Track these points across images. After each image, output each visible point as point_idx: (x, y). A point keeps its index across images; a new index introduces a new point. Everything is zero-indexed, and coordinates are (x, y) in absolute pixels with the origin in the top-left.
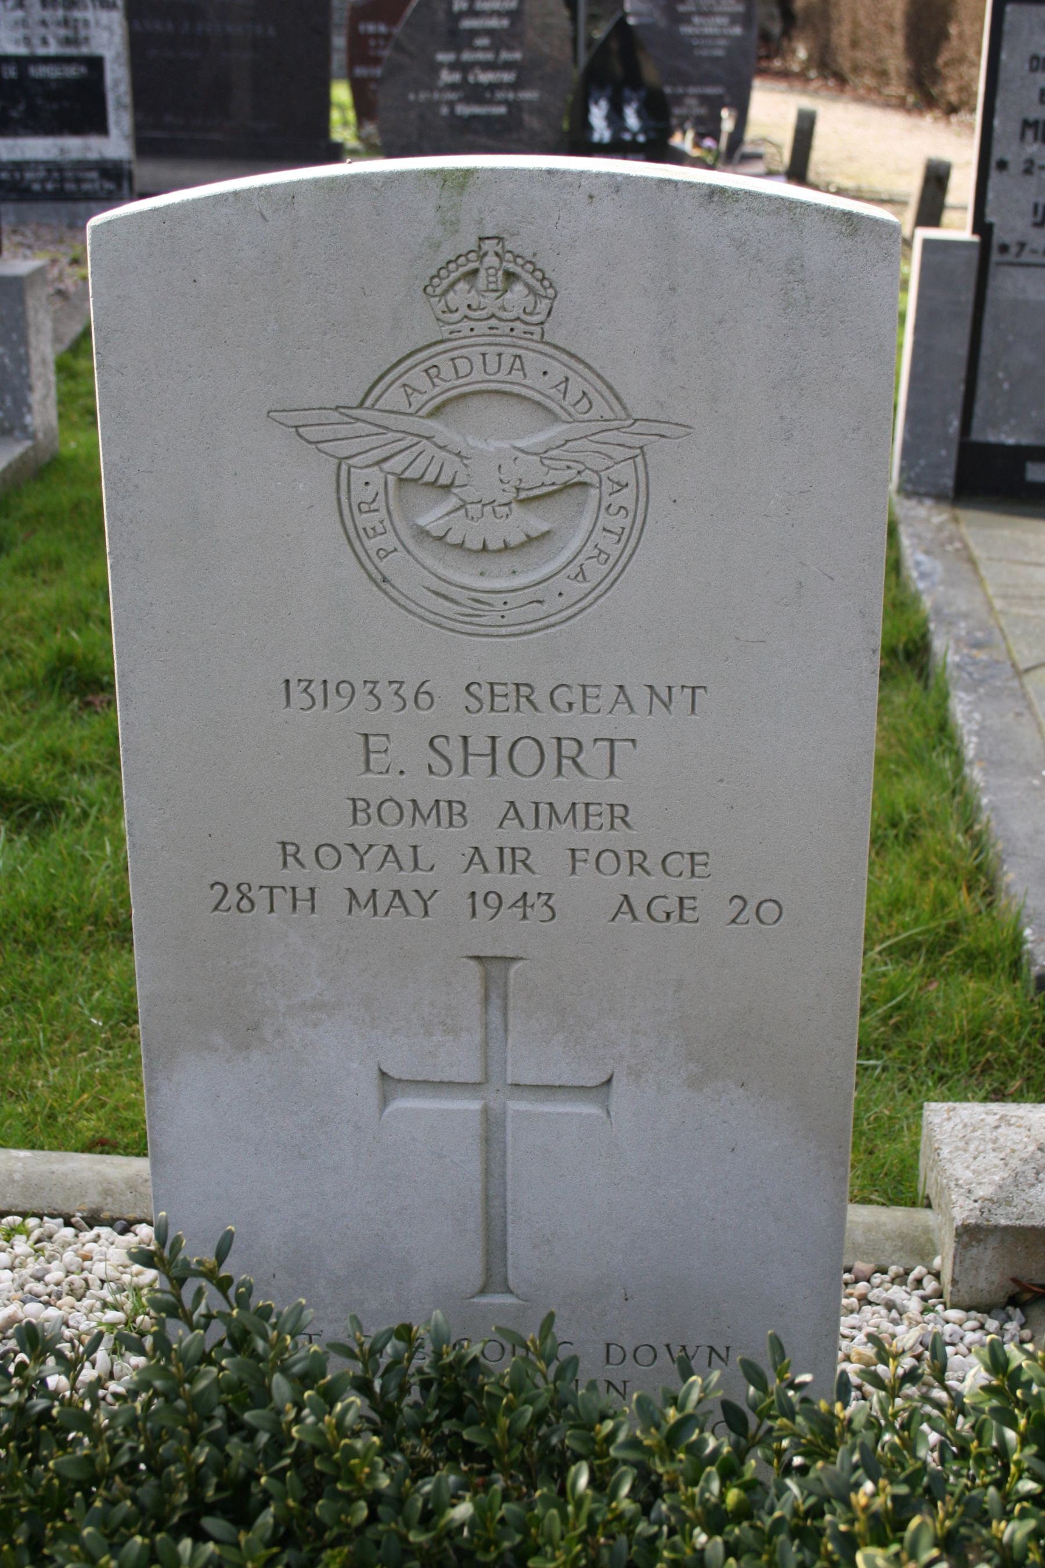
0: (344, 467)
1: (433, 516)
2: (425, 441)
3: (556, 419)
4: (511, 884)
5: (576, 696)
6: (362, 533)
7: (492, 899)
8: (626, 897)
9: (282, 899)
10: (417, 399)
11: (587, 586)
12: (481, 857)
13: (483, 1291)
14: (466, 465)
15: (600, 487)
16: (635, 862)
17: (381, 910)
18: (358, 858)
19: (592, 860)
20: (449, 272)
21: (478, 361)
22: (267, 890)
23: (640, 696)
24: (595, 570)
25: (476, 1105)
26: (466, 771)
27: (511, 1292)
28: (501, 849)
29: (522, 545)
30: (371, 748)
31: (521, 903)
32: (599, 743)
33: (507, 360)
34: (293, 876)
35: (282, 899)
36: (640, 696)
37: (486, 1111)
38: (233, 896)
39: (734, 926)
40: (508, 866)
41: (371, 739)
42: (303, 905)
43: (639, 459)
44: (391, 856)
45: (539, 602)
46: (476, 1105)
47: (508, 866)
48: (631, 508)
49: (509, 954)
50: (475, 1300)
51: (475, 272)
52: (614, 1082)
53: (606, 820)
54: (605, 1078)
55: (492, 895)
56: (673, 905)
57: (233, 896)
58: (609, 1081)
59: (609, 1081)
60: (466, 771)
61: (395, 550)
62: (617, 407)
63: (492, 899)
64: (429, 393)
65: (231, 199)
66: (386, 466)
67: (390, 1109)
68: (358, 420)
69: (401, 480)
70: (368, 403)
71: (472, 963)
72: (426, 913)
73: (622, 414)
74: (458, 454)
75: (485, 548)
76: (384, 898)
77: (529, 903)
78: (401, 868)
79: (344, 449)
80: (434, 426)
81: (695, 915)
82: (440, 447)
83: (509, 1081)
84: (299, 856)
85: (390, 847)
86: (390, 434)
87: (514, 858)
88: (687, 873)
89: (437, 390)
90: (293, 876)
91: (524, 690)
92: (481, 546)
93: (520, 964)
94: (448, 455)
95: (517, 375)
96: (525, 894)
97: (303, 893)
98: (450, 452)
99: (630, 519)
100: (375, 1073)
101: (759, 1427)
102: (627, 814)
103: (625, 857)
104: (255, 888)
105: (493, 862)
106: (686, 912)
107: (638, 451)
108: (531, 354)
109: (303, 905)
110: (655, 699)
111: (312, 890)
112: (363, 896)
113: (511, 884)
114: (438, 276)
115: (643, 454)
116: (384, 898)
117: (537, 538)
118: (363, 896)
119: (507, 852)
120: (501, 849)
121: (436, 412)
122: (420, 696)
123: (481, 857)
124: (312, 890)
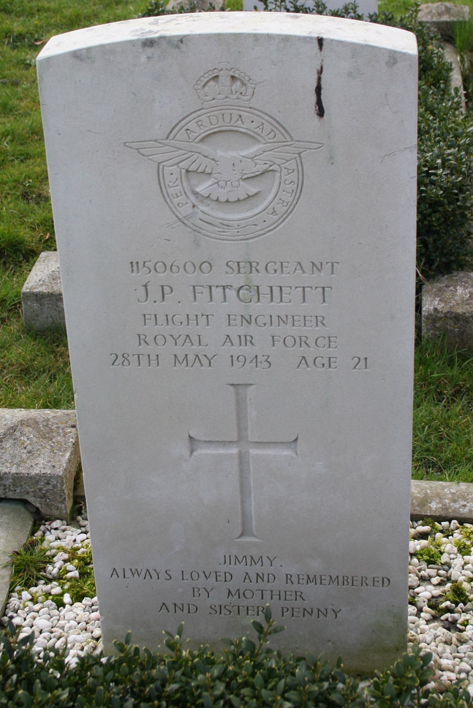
0: (161, 167)
1: (202, 188)
2: (197, 154)
3: (259, 142)
4: (249, 351)
5: (278, 266)
6: (170, 196)
7: (242, 359)
8: (304, 357)
9: (144, 360)
10: (193, 135)
11: (277, 217)
12: (230, 340)
14: (218, 165)
15: (281, 173)
21: (220, 118)
23: (307, 266)
24: (281, 209)
28: (240, 336)
29: (245, 199)
32: (297, 289)
33: (235, 118)
34: (143, 349)
35: (144, 360)
36: (307, 266)
37: (240, 452)
38: (120, 359)
39: (355, 370)
42: (154, 362)
43: (298, 159)
45: (255, 225)
46: (234, 451)
48: (296, 182)
51: (217, 77)
52: (299, 440)
53: (302, 322)
56: (326, 361)
57: (120, 359)
58: (296, 439)
59: (296, 439)
61: (187, 203)
62: (286, 135)
63: (242, 359)
64: (199, 132)
66: (181, 165)
67: (195, 454)
68: (166, 145)
69: (187, 171)
70: (172, 136)
71: (232, 388)
73: (289, 139)
74: (213, 160)
75: (217, 200)
76: (191, 358)
79: (159, 158)
80: (203, 147)
82: (204, 156)
84: (253, 341)
85: (188, 336)
86: (181, 151)
87: (247, 340)
88: (327, 346)
89: (202, 131)
90: (143, 349)
92: (216, 199)
94: (208, 160)
95: (240, 122)
96: (256, 356)
97: (153, 357)
98: (210, 159)
99: (296, 186)
100: (188, 436)
101: (268, 629)
103: (298, 340)
104: (131, 355)
107: (297, 155)
108: (246, 114)
109: (154, 362)
110: (314, 268)
112: (181, 358)
113: (249, 351)
115: (300, 157)
116: (191, 358)
117: (253, 196)
118: (181, 358)
120: (240, 336)
121: (202, 140)
122: (173, 267)
123: (230, 340)
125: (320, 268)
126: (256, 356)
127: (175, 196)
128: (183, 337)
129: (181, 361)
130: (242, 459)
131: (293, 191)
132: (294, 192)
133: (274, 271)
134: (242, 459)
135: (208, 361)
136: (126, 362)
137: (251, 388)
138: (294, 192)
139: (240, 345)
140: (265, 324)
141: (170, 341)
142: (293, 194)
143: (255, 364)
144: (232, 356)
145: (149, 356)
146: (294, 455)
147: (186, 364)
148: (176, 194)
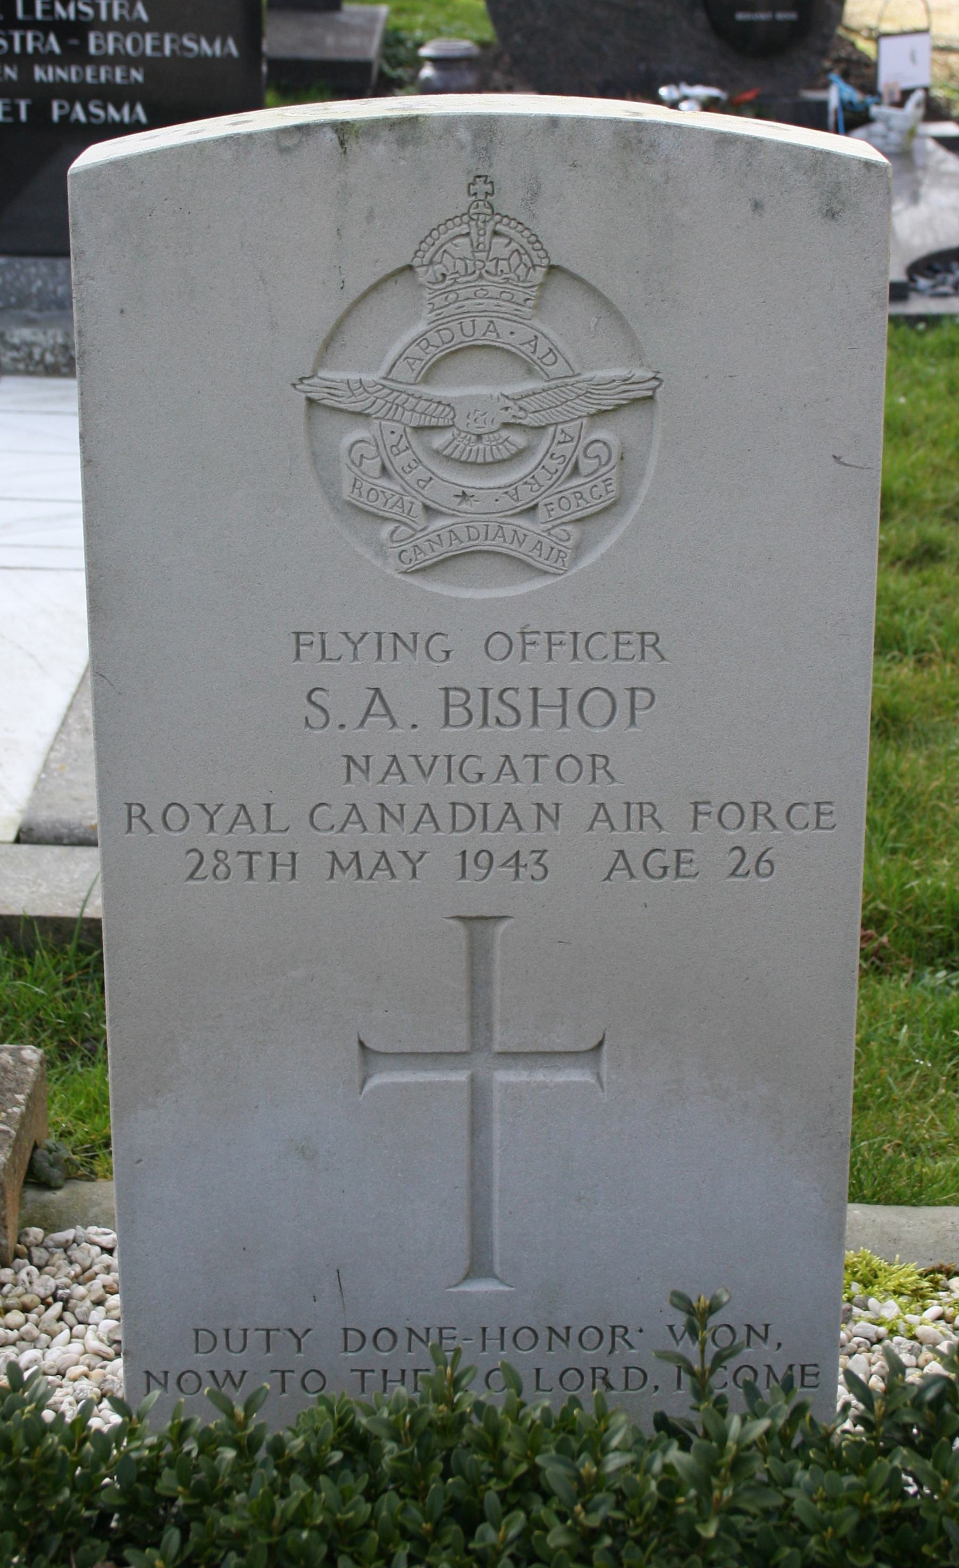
3: (530, 372)
9: (262, 863)
13: (467, 1277)
16: (760, 811)
17: (366, 873)
18: (207, 818)
19: (715, 817)
20: (448, 229)
22: (246, 856)
25: (461, 1077)
26: (535, 722)
27: (496, 1278)
30: (451, 702)
31: (512, 862)
37: (472, 1079)
40: (635, 824)
41: (451, 693)
42: (283, 871)
44: (510, 817)
46: (461, 1077)
47: (635, 824)
49: (485, 912)
50: (461, 1288)
52: (605, 1047)
54: (595, 1042)
55: (484, 854)
56: (669, 859)
59: (601, 1044)
60: (535, 722)
65: (464, 135)
72: (414, 875)
77: (522, 862)
78: (438, 829)
81: (693, 869)
83: (497, 1048)
84: (656, 815)
88: (813, 824)
91: (650, 639)
93: (511, 921)
102: (607, 763)
105: (618, 818)
106: (683, 866)
109: (283, 871)
111: (294, 855)
112: (345, 857)
114: (437, 229)
118: (345, 857)
119: (635, 808)
124: (294, 855)
125: (411, 646)
126: (518, 853)
127: (408, 469)
128: (229, 811)
129: (345, 865)
130: (478, 1093)
131: (557, 470)
132: (558, 474)
133: (444, 654)
134: (478, 1093)
135: (409, 867)
136: (222, 869)
137: (502, 927)
138: (558, 474)
139: (629, 828)
140: (481, 775)
141: (199, 819)
142: (555, 477)
143: (513, 870)
144: (464, 853)
145: (274, 855)
146: (592, 1080)
147: (356, 873)
148: (409, 466)
